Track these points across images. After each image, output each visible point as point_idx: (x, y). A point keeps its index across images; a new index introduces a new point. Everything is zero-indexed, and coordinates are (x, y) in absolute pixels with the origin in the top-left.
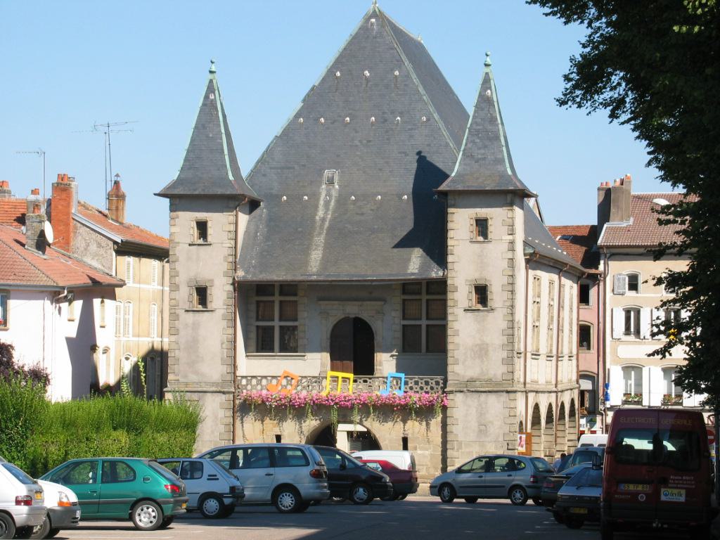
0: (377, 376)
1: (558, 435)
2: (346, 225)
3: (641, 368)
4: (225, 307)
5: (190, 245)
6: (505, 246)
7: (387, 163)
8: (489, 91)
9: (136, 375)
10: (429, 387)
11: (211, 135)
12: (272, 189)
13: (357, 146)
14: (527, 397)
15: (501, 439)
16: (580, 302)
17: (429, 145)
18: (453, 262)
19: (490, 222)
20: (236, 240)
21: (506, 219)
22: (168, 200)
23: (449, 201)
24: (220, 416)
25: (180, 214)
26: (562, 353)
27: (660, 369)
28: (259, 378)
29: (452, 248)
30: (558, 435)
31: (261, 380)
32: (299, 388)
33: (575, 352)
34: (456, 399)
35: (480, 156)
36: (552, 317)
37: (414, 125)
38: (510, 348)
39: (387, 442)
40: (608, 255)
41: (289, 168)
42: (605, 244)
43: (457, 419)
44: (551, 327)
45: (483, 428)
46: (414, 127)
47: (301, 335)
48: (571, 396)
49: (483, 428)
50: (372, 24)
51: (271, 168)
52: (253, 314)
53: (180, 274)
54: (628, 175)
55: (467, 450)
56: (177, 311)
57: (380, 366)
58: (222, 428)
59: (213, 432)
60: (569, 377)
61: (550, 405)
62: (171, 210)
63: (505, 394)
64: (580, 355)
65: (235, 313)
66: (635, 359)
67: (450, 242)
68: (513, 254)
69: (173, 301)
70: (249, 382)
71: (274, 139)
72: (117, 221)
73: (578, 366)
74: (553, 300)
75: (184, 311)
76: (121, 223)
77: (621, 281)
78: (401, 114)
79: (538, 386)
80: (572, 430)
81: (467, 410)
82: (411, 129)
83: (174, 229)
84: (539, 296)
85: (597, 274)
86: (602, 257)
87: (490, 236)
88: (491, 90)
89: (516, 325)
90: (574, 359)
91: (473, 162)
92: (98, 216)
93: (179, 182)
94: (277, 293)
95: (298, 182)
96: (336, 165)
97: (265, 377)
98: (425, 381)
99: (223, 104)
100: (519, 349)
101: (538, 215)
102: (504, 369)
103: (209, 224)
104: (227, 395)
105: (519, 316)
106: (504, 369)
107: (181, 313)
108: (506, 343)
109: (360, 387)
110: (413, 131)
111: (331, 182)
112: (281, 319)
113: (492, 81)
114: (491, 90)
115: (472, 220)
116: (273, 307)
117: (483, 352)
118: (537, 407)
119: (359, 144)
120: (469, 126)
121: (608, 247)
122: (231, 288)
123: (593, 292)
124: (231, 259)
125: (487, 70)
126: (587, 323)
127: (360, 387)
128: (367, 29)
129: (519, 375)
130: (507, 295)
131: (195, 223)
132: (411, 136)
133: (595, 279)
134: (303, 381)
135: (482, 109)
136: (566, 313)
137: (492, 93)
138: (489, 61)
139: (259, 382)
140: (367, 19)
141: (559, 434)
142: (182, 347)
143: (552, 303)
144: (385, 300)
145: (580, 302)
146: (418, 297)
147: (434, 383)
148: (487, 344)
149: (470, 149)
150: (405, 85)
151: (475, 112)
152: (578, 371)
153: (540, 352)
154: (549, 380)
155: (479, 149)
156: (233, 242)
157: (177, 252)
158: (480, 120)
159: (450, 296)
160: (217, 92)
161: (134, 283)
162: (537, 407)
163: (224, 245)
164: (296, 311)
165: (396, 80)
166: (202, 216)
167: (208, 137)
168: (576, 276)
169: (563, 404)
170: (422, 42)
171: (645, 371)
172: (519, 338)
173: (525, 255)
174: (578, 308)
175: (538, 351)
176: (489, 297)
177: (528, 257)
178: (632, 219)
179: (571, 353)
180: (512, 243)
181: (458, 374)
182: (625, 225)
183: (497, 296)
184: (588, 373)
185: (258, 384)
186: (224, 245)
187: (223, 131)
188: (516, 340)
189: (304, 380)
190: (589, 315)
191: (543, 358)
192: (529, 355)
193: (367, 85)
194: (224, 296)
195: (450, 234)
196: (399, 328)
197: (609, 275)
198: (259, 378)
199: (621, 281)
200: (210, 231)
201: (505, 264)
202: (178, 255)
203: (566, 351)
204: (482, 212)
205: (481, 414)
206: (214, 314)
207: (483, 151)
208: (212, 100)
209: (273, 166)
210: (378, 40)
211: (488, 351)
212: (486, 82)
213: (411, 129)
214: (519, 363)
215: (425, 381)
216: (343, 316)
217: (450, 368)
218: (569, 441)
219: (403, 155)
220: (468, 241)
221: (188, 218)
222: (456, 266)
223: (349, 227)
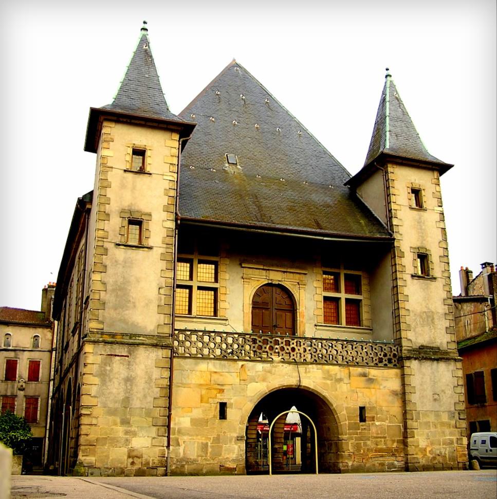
4: (165, 246)
5: (125, 171)
18: (398, 226)
21: (435, 192)
24: (154, 377)
34: (412, 366)
39: (344, 412)
45: (436, 396)
49: (436, 396)
53: (112, 202)
55: (425, 420)
58: (157, 392)
59: (145, 396)
81: (423, 378)
92: (8, 331)
108: (447, 312)
138: (146, 26)
142: (109, 288)
163: (165, 177)
186: (165, 177)
194: (164, 233)
202: (109, 180)
206: (151, 252)
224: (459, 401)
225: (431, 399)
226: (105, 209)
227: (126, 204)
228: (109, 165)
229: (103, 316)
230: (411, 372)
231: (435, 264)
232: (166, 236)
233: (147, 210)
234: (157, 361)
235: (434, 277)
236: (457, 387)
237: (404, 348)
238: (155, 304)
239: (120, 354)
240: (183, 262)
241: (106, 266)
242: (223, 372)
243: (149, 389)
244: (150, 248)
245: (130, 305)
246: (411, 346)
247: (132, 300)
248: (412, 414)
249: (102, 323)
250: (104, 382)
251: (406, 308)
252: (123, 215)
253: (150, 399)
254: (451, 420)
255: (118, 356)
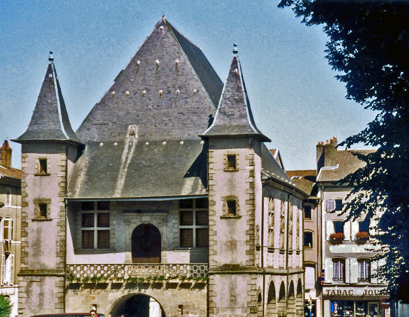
0: (162, 263)
1: (289, 303)
2: (142, 161)
3: (345, 259)
4: (59, 217)
6: (248, 174)
7: (170, 120)
8: (236, 69)
9: (13, 265)
10: (194, 272)
11: (50, 102)
12: (94, 138)
13: (150, 109)
14: (264, 278)
15: (246, 306)
16: (306, 217)
17: (198, 108)
19: (237, 157)
20: (66, 172)
21: (248, 155)
22: (20, 145)
23: (209, 143)
25: (29, 154)
26: (291, 248)
27: (356, 259)
28: (82, 266)
29: (211, 175)
30: (289, 303)
31: (83, 267)
32: (109, 272)
33: (301, 248)
35: (230, 113)
36: (284, 224)
37: (188, 94)
38: (251, 243)
39: (168, 309)
40: (323, 188)
41: (105, 124)
42: (321, 180)
43: (216, 292)
44: (283, 231)
45: (234, 298)
46: (188, 96)
47: (112, 236)
48: (298, 276)
49: (234, 298)
50: (161, 29)
51: (93, 125)
52: (80, 222)
53: (29, 196)
54: (335, 137)
56: (26, 221)
57: (165, 256)
60: (297, 265)
61: (283, 283)
62: (23, 152)
63: (248, 275)
64: (305, 252)
65: (66, 221)
66: (340, 254)
67: (210, 171)
68: (254, 179)
69: (24, 214)
70: (75, 268)
71: (96, 105)
72: (6, 167)
73: (303, 258)
74: (284, 213)
75: (31, 220)
76: (9, 168)
77: (331, 204)
78: (180, 88)
79: (273, 270)
80: (300, 299)
82: (186, 98)
83: (25, 165)
84: (273, 210)
85: (316, 200)
86: (319, 189)
87: (238, 167)
88: (238, 69)
89: (255, 228)
90: (301, 255)
91: (226, 117)
93: (28, 133)
94: (96, 207)
95: (111, 133)
96: (137, 122)
97: (86, 265)
98: (194, 267)
99: (59, 81)
100: (258, 244)
101: (280, 165)
102: (248, 258)
103: (48, 161)
104: (60, 277)
105: (258, 221)
106: (248, 258)
107: (29, 221)
109: (150, 271)
110: (188, 99)
111: (133, 134)
112: (99, 225)
113: (238, 63)
114: (238, 69)
115: (225, 156)
116: (93, 217)
117: (233, 246)
118: (272, 285)
119: (151, 108)
120: (223, 93)
121: (323, 182)
122: (63, 205)
123: (313, 212)
124: (63, 185)
125: (235, 55)
126: (310, 231)
127: (150, 271)
128: (158, 33)
129: (258, 262)
130: (249, 207)
131: (39, 161)
132: (186, 102)
133: (316, 203)
134: (112, 267)
135: (232, 82)
136: (294, 223)
137: (238, 70)
138: (236, 49)
139: (102, 268)
140: (158, 26)
141: (289, 302)
142: (30, 245)
143: (283, 215)
144: (167, 212)
145: (306, 217)
146: (190, 210)
147: (200, 268)
148: (236, 241)
149: (224, 108)
150: (183, 69)
151: (227, 83)
152: (304, 261)
153: (275, 247)
154: (281, 266)
155: (230, 108)
156: (64, 173)
157: (26, 181)
158: (230, 89)
159: (210, 208)
160: (54, 73)
161: (12, 205)
162: (272, 285)
164: (109, 220)
165: (177, 66)
166: (43, 156)
167: (47, 102)
168: (301, 199)
169: (292, 282)
170: (200, 48)
171: (347, 261)
172: (259, 237)
173: (262, 180)
174: (303, 222)
175: (273, 246)
176: (237, 209)
177: (264, 182)
178: (338, 165)
179: (298, 249)
180: (252, 172)
181: (217, 262)
182: (333, 169)
183: (243, 208)
184: (311, 263)
185: (81, 270)
187: (58, 98)
188: (256, 238)
189: (112, 267)
190: (310, 226)
191: (277, 252)
192: (266, 250)
193: (157, 69)
194: (58, 210)
195: (211, 166)
196: (177, 231)
197: (324, 200)
198: (82, 266)
199: (331, 204)
200: (48, 166)
201: (248, 186)
202: (27, 182)
203: (294, 247)
204: (232, 151)
205: (232, 289)
207: (232, 110)
208: (51, 78)
209: (94, 123)
210: (165, 40)
211: (236, 245)
212: (235, 63)
213: (186, 98)
214: (258, 254)
215: (194, 267)
216: (140, 223)
217: (211, 258)
218: (297, 306)
219: (181, 115)
220: (222, 171)
221: (34, 158)
222: (214, 188)
223: (144, 162)
224: (252, 301)
225: (229, 299)
226: (25, 200)
227: (36, 196)
228: (26, 172)
229: (27, 261)
230: (214, 283)
231: (241, 207)
232: (59, 211)
233: (47, 198)
234: (56, 283)
235: (240, 216)
236: (250, 291)
237: (211, 267)
238: (55, 250)
239: (36, 281)
240: (208, 218)
241: (27, 233)
242: (339, 286)
243: (52, 299)
244: (51, 220)
245: (41, 253)
246: (216, 265)
247: (42, 251)
248: (213, 310)
249: (26, 264)
250: (28, 297)
251: (214, 240)
252: (35, 202)
253: (53, 304)
254: (243, 313)
255: (36, 282)
